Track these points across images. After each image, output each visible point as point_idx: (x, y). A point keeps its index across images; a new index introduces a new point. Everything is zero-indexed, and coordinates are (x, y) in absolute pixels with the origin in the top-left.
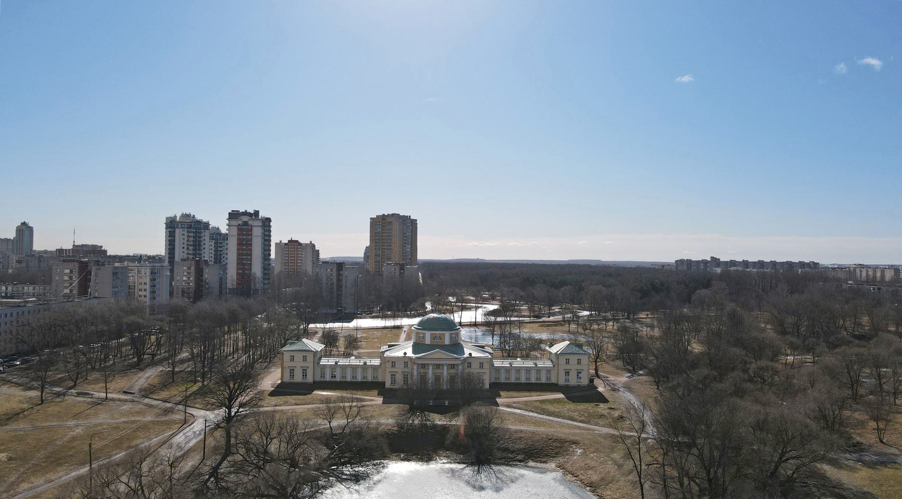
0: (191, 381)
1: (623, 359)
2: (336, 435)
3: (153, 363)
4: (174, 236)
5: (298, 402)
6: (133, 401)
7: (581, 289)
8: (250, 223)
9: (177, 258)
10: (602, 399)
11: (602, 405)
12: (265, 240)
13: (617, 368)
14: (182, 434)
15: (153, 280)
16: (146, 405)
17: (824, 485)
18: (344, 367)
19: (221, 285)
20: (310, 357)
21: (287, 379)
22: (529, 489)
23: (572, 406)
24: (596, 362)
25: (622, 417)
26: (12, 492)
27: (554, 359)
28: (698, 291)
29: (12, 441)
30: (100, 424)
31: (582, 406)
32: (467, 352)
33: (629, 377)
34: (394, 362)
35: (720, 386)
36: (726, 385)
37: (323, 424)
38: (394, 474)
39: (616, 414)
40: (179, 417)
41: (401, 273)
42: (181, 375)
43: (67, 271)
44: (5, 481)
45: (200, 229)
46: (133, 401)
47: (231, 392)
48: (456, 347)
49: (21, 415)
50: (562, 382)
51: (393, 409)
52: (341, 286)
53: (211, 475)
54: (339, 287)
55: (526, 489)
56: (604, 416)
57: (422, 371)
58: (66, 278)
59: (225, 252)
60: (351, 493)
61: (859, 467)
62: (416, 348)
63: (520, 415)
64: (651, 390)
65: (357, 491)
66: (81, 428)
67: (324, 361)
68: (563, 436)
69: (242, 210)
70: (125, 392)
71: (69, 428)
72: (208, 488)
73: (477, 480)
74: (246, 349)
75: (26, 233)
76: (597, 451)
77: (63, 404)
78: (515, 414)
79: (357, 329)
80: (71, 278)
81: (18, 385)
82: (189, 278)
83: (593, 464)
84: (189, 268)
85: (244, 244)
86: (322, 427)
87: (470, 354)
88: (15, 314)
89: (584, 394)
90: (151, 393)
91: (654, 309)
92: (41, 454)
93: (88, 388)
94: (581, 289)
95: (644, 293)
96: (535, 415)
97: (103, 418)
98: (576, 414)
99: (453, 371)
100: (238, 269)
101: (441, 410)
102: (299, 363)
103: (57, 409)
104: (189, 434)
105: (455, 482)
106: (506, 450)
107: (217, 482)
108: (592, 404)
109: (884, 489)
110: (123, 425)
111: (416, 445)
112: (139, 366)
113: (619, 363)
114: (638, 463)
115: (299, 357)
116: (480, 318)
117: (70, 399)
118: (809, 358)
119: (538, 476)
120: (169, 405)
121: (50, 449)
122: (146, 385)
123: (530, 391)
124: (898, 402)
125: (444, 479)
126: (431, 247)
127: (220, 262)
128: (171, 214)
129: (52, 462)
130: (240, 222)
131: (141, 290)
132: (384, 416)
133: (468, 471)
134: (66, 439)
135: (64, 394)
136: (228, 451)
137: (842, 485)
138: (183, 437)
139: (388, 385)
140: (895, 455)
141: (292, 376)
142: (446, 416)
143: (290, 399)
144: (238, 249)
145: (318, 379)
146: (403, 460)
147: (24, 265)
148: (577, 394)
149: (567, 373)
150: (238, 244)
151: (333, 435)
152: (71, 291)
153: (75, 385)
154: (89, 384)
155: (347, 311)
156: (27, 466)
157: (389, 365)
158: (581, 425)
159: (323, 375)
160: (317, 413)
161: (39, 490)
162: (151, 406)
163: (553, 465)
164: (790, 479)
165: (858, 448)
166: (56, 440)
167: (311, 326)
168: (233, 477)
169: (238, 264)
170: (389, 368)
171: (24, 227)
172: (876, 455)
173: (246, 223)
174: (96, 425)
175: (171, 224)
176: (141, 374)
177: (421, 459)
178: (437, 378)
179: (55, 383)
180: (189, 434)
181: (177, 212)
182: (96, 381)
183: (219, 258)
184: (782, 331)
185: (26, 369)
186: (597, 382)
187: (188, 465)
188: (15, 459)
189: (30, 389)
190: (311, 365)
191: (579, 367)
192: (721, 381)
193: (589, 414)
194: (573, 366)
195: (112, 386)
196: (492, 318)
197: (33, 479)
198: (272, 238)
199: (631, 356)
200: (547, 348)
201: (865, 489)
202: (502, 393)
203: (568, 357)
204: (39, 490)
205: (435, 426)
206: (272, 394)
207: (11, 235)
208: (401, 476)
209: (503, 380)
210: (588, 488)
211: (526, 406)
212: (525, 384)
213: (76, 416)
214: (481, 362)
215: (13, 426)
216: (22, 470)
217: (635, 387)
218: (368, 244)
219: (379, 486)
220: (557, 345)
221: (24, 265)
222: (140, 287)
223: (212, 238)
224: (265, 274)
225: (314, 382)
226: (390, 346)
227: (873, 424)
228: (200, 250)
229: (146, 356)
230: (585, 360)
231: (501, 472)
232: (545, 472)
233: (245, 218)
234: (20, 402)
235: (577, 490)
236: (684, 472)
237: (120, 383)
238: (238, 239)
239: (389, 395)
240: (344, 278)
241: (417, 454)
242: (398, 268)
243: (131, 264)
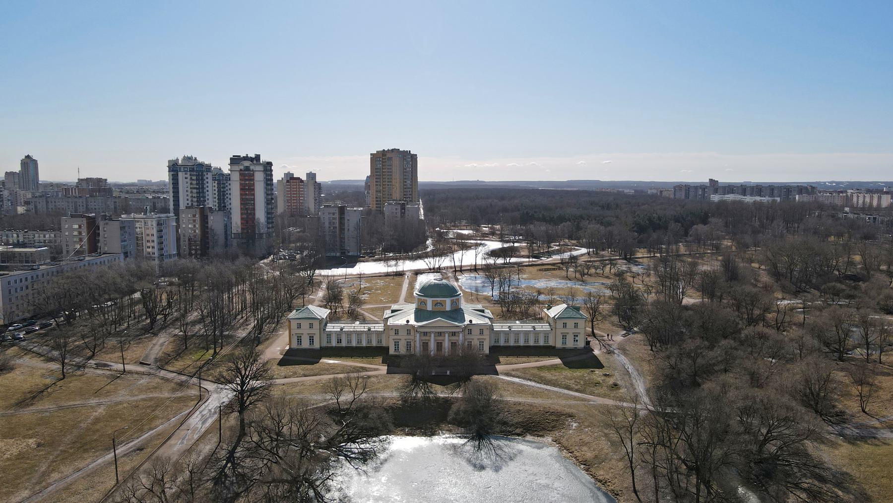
0: (203, 348)
5: (307, 373)
6: (149, 374)
8: (251, 168)
9: (182, 206)
10: (597, 364)
11: (597, 371)
12: (267, 185)
14: (198, 412)
15: (160, 231)
17: (805, 464)
18: (349, 334)
20: (316, 325)
21: (295, 345)
23: (568, 373)
24: (592, 321)
26: (44, 484)
29: (39, 425)
30: (121, 403)
31: (579, 373)
32: (468, 318)
33: (624, 336)
34: (397, 330)
35: (711, 354)
37: (330, 399)
39: (611, 381)
40: (194, 392)
41: (402, 213)
43: (76, 226)
46: (149, 374)
47: (242, 378)
48: (457, 314)
49: (45, 393)
50: (559, 345)
51: (397, 380)
54: (342, 229)
55: (524, 467)
56: (599, 383)
58: (76, 233)
59: (228, 192)
61: (840, 442)
62: (420, 314)
65: (365, 472)
66: (103, 407)
67: (330, 327)
68: (559, 408)
69: (243, 155)
70: (141, 363)
71: (92, 407)
72: (226, 476)
75: (31, 165)
77: (84, 378)
78: (513, 383)
80: (80, 233)
81: (39, 355)
82: (195, 226)
84: (194, 216)
85: (247, 189)
88: (29, 278)
89: (581, 359)
90: (167, 363)
91: (651, 247)
92: (68, 439)
96: (533, 384)
98: (573, 381)
100: (242, 214)
101: (443, 381)
102: (305, 330)
104: (204, 413)
106: (505, 423)
107: (234, 468)
108: (588, 371)
109: (862, 469)
111: (418, 418)
112: (151, 330)
113: (615, 319)
114: (629, 450)
115: (305, 324)
116: (480, 262)
117: (90, 372)
119: (536, 451)
120: (184, 378)
121: (76, 432)
122: (160, 354)
123: (528, 355)
129: (79, 448)
130: (242, 167)
131: (148, 241)
132: (386, 387)
134: (89, 421)
135: (84, 366)
136: (242, 430)
137: (822, 464)
138: (200, 416)
139: (392, 351)
140: (876, 428)
142: (448, 390)
143: (299, 369)
145: (324, 344)
146: (407, 435)
147: (32, 206)
148: (574, 359)
149: (564, 337)
150: (241, 189)
154: (106, 353)
155: (350, 254)
156: (56, 453)
158: (577, 394)
160: (326, 389)
161: (69, 480)
163: (550, 439)
165: (840, 418)
166: (80, 422)
167: (317, 272)
168: (248, 462)
170: (393, 336)
171: (28, 160)
172: (857, 428)
173: (247, 169)
175: (174, 167)
177: (425, 434)
179: (77, 352)
180: (204, 413)
181: (179, 155)
182: (113, 349)
183: (223, 206)
184: (776, 274)
185: (46, 335)
186: (594, 343)
187: (206, 448)
195: (128, 355)
197: (62, 468)
199: (627, 310)
200: (545, 310)
201: (844, 469)
202: (502, 359)
206: (282, 363)
208: (406, 453)
209: (502, 343)
210: (582, 466)
211: (525, 374)
213: (97, 393)
214: (481, 329)
215: (39, 406)
217: (629, 347)
219: (386, 466)
221: (32, 206)
222: (148, 238)
223: (214, 179)
224: (268, 218)
226: (393, 311)
228: (203, 192)
229: (158, 317)
231: (501, 448)
232: (542, 448)
233: (247, 163)
234: (43, 376)
235: (573, 468)
237: (136, 351)
238: (241, 184)
239: (394, 363)
241: (421, 428)
242: (399, 207)
243: (137, 216)
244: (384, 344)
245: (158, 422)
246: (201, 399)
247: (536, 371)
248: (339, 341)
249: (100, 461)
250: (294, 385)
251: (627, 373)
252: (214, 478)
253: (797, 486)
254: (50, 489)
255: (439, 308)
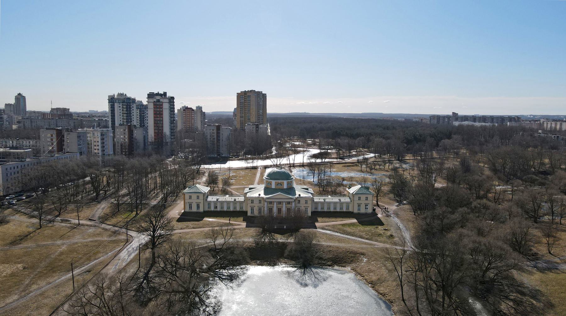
0: (129, 211)
2: (218, 249)
3: (105, 198)
4: (114, 108)
5: (195, 226)
6: (95, 226)
7: (369, 140)
8: (161, 100)
10: (380, 223)
11: (380, 227)
12: (171, 111)
13: (390, 199)
14: (125, 249)
15: (102, 139)
16: (103, 229)
17: (512, 285)
18: (222, 203)
20: (201, 197)
21: (187, 210)
23: (361, 228)
24: (377, 197)
26: (27, 291)
27: (351, 196)
30: (77, 243)
31: (368, 228)
32: (298, 193)
33: (397, 206)
34: (252, 200)
35: (453, 216)
36: (456, 216)
37: (210, 242)
38: (254, 275)
40: (123, 237)
42: (123, 206)
43: (49, 135)
44: (22, 284)
45: (130, 103)
47: (154, 227)
48: (291, 190)
49: (29, 237)
50: (356, 211)
51: (253, 231)
52: (219, 140)
54: (218, 140)
55: (332, 285)
57: (269, 205)
59: (146, 119)
61: (535, 271)
62: (267, 191)
64: (410, 215)
65: (232, 287)
66: (65, 246)
67: (210, 199)
69: (156, 92)
70: (90, 219)
71: (59, 246)
72: (143, 288)
73: (303, 279)
74: (163, 186)
76: (376, 260)
77: (53, 228)
78: (326, 234)
79: (230, 169)
80: (52, 140)
81: (25, 214)
83: (373, 268)
84: (125, 130)
85: (158, 114)
86: (210, 244)
88: (19, 167)
89: (369, 220)
90: (106, 220)
91: (415, 154)
92: (43, 264)
93: (67, 216)
94: (369, 140)
95: (409, 142)
96: (339, 234)
97: (78, 239)
98: (364, 233)
100: (155, 130)
101: (282, 232)
102: (194, 200)
103: (50, 232)
105: (291, 280)
106: (321, 259)
107: (148, 283)
109: (549, 288)
110: (90, 244)
111: (265, 255)
112: (97, 200)
113: (392, 196)
115: (194, 196)
116: (306, 161)
118: (509, 187)
119: (340, 275)
120: (117, 229)
121: (48, 261)
122: (102, 214)
125: (284, 279)
126: (275, 106)
128: (111, 94)
130: (155, 100)
131: (95, 146)
134: (57, 254)
135: (53, 221)
136: (153, 262)
137: (523, 284)
138: (127, 252)
139: (249, 214)
141: (190, 207)
142: (286, 238)
143: (190, 224)
144: (154, 117)
145: (206, 209)
146: (259, 265)
150: (154, 114)
152: (53, 148)
153: (60, 214)
157: (250, 202)
158: (367, 241)
159: (209, 207)
160: (207, 236)
161: (43, 289)
162: (106, 230)
163: (349, 269)
164: (493, 280)
165: (535, 257)
168: (157, 280)
169: (154, 126)
170: (250, 204)
171: (19, 97)
172: (545, 263)
173: (158, 101)
174: (74, 244)
175: (112, 100)
176: (98, 206)
177: (269, 265)
180: (129, 250)
181: (115, 92)
182: (72, 211)
183: (142, 119)
184: (495, 170)
185: (29, 202)
186: (378, 210)
187: (132, 270)
190: (202, 201)
191: (367, 202)
192: (453, 214)
193: (372, 233)
194: (363, 201)
195: (82, 214)
196: (313, 160)
199: (399, 190)
200: (347, 189)
201: (537, 288)
202: (319, 219)
203: (360, 196)
205: (278, 243)
206: (179, 220)
207: (12, 101)
208: (258, 276)
209: (319, 209)
210: (370, 285)
212: (333, 212)
213: (62, 237)
214: (306, 200)
215: (25, 245)
216: (32, 276)
218: (236, 107)
219: (245, 283)
220: (354, 180)
221: (21, 125)
222: (95, 144)
223: (137, 108)
224: (171, 133)
226: (250, 189)
227: (544, 240)
230: (370, 197)
231: (318, 274)
232: (344, 273)
233: (158, 98)
234: (27, 226)
235: (364, 286)
236: (428, 277)
237: (86, 212)
238: (154, 111)
239: (250, 221)
240: (221, 135)
241: (267, 261)
242: (255, 126)
243: (88, 129)
245: (100, 255)
246: (128, 241)
247: (340, 227)
248: (216, 207)
250: (187, 233)
251: (399, 228)
252: (135, 289)
255: (279, 187)
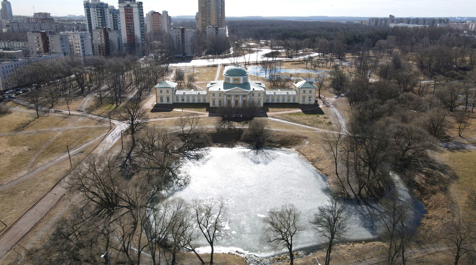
1: (334, 88)
3: (89, 92)
6: (83, 116)
8: (131, 5)
9: (93, 28)
11: (321, 116)
12: (140, 15)
13: (330, 92)
14: (110, 135)
16: (90, 118)
17: (425, 161)
18: (188, 96)
19: (119, 42)
20: (170, 91)
21: (159, 102)
22: (282, 163)
23: (305, 116)
24: (319, 90)
25: (330, 123)
27: (297, 90)
28: (379, 41)
30: (69, 130)
32: (252, 87)
33: (336, 98)
34: (214, 94)
35: (382, 107)
36: (385, 106)
37: (179, 129)
39: (328, 121)
40: (107, 125)
43: (35, 38)
45: (103, 8)
47: (132, 116)
48: (246, 85)
49: (29, 125)
50: (301, 102)
51: (214, 120)
52: (184, 41)
53: (127, 158)
54: (183, 42)
55: (280, 163)
56: (321, 122)
57: (228, 98)
59: (119, 22)
60: (195, 165)
61: (445, 151)
62: (226, 85)
63: (278, 122)
66: (60, 132)
67: (178, 92)
70: (78, 111)
71: (55, 132)
72: (127, 165)
74: (137, 83)
78: (276, 121)
79: (194, 67)
80: (38, 42)
81: (24, 106)
83: (313, 149)
84: (101, 33)
85: (129, 18)
86: (179, 130)
87: (254, 89)
88: (13, 65)
89: (312, 109)
90: (92, 111)
91: (353, 53)
92: (44, 147)
94: (314, 41)
96: (286, 122)
97: (70, 126)
98: (307, 121)
99: (244, 98)
100: (127, 32)
101: (239, 120)
102: (165, 94)
106: (271, 142)
107: (130, 162)
108: (316, 115)
109: (455, 163)
111: (225, 139)
112: (82, 94)
113: (332, 89)
115: (164, 91)
116: (260, 59)
119: (287, 155)
121: (48, 144)
122: (88, 106)
124: (474, 110)
127: (117, 29)
130: (125, 5)
131: (76, 47)
132: (208, 123)
133: (252, 153)
134: (54, 138)
135: (48, 112)
136: (133, 145)
138: (111, 137)
139: (211, 105)
140: (465, 144)
143: (162, 114)
144: (126, 21)
145: (175, 102)
146: (220, 147)
149: (304, 98)
150: (126, 18)
151: (184, 134)
152: (40, 49)
153: (53, 106)
156: (39, 153)
158: (309, 127)
159: (178, 100)
160: (176, 123)
161: (47, 166)
162: (93, 119)
164: (410, 158)
169: (127, 29)
170: (212, 97)
172: (455, 144)
178: (237, 102)
180: (113, 135)
183: (116, 27)
184: (421, 67)
185: (26, 96)
188: (32, 150)
189: (30, 108)
190: (171, 95)
194: (307, 94)
195: (71, 106)
198: (144, 11)
199: (339, 85)
200: (294, 84)
201: (446, 164)
202: (270, 109)
203: (304, 89)
204: (47, 166)
205: (235, 129)
206: (153, 111)
211: (282, 117)
213: (57, 125)
214: (259, 93)
215: (27, 131)
216: (37, 155)
217: (339, 104)
218: (198, 11)
219: (209, 162)
221: (10, 28)
222: (76, 45)
223: (110, 13)
224: (142, 35)
225: (173, 103)
226: (212, 84)
227: (457, 126)
228: (105, 20)
231: (268, 154)
234: (27, 116)
237: (75, 105)
238: (125, 15)
239: (212, 111)
241: (227, 144)
242: (215, 29)
243: (69, 32)
244: (207, 102)
245: (89, 139)
247: (288, 116)
248: (183, 100)
249: (62, 157)
251: (337, 117)
253: (420, 171)
254: (38, 170)
255: (236, 82)
